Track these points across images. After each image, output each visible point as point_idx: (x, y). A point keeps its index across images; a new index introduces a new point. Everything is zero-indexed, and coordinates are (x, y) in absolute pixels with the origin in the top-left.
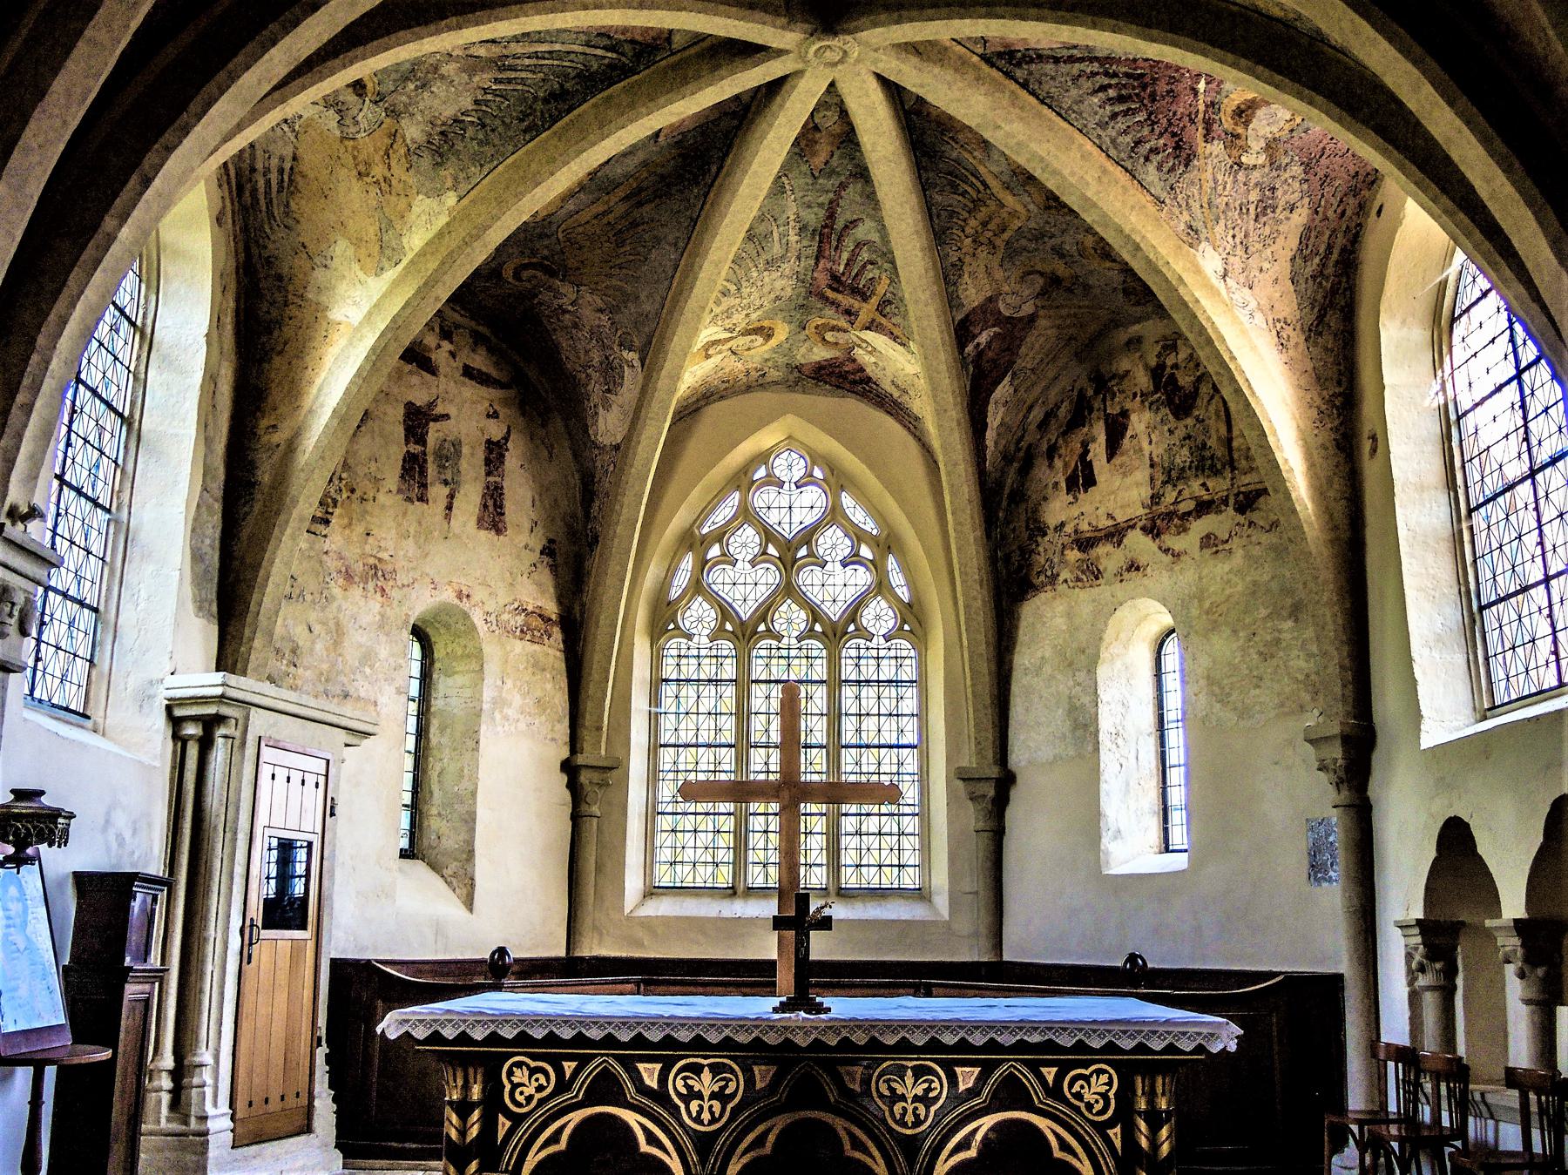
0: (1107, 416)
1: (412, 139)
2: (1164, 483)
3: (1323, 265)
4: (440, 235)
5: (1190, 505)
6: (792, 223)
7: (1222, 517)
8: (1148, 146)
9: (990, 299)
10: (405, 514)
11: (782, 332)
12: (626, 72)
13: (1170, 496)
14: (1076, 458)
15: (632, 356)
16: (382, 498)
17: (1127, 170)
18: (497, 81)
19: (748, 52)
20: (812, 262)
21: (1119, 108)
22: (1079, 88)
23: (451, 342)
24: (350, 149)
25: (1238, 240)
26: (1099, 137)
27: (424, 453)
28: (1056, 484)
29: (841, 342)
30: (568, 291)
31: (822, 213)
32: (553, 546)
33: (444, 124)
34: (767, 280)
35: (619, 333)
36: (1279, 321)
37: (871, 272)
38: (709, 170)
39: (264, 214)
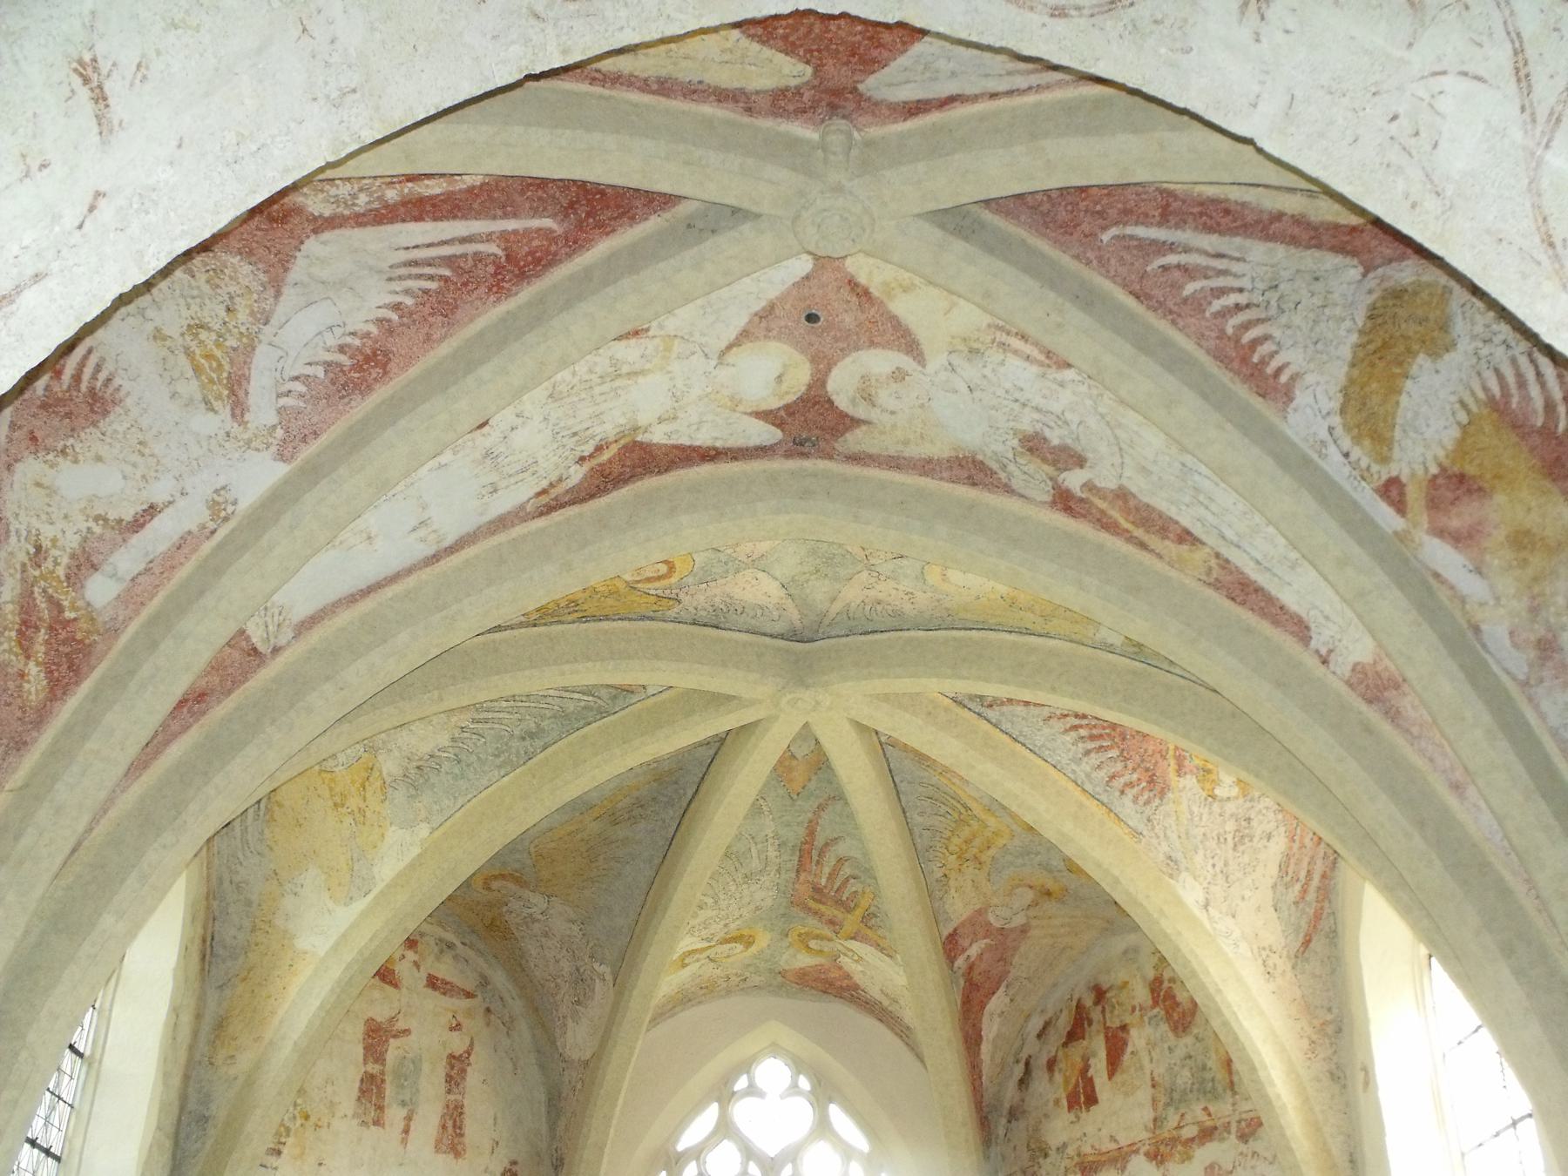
0: (1107, 1029)
1: (390, 775)
2: (1167, 1105)
3: (1304, 891)
4: (412, 866)
5: (1190, 1132)
6: (771, 841)
7: (1225, 1145)
8: (1122, 780)
9: (980, 912)
10: (360, 1140)
11: (763, 940)
12: (603, 713)
13: (1173, 1120)
14: (1076, 1072)
15: (605, 969)
16: (337, 1123)
17: (1103, 804)
18: (474, 721)
19: (718, 701)
20: (793, 875)
21: (1091, 745)
22: (1051, 728)
23: (416, 952)
24: (326, 781)
25: (1218, 869)
26: (1074, 772)
27: (383, 1073)
28: (1057, 1102)
29: (826, 950)
30: (538, 901)
31: (802, 832)
32: (514, 1168)
33: (421, 759)
34: (746, 892)
35: (591, 945)
36: (1264, 949)
37: (854, 886)
38: (685, 794)
39: (238, 840)
